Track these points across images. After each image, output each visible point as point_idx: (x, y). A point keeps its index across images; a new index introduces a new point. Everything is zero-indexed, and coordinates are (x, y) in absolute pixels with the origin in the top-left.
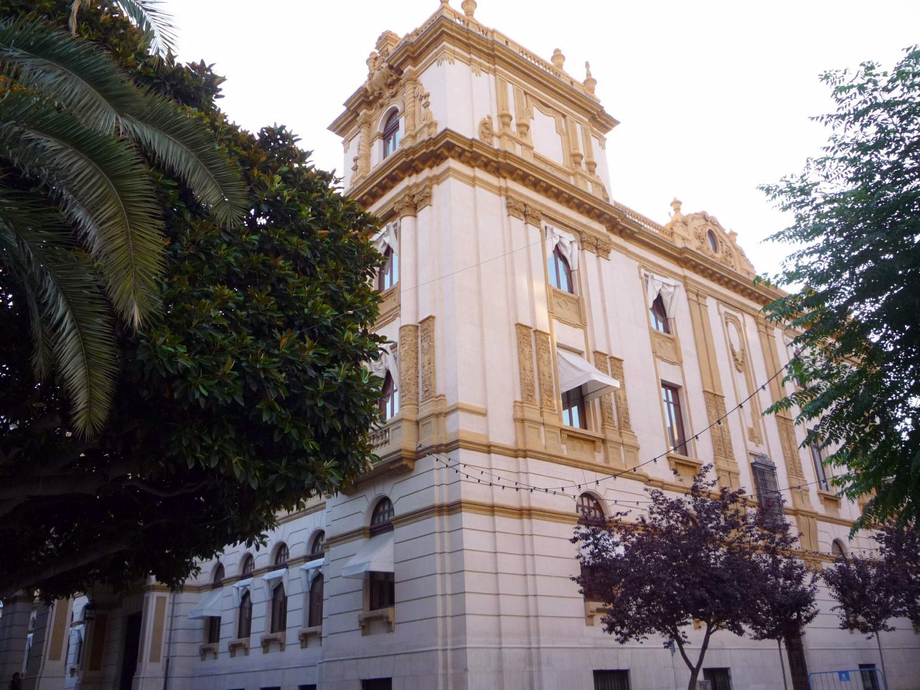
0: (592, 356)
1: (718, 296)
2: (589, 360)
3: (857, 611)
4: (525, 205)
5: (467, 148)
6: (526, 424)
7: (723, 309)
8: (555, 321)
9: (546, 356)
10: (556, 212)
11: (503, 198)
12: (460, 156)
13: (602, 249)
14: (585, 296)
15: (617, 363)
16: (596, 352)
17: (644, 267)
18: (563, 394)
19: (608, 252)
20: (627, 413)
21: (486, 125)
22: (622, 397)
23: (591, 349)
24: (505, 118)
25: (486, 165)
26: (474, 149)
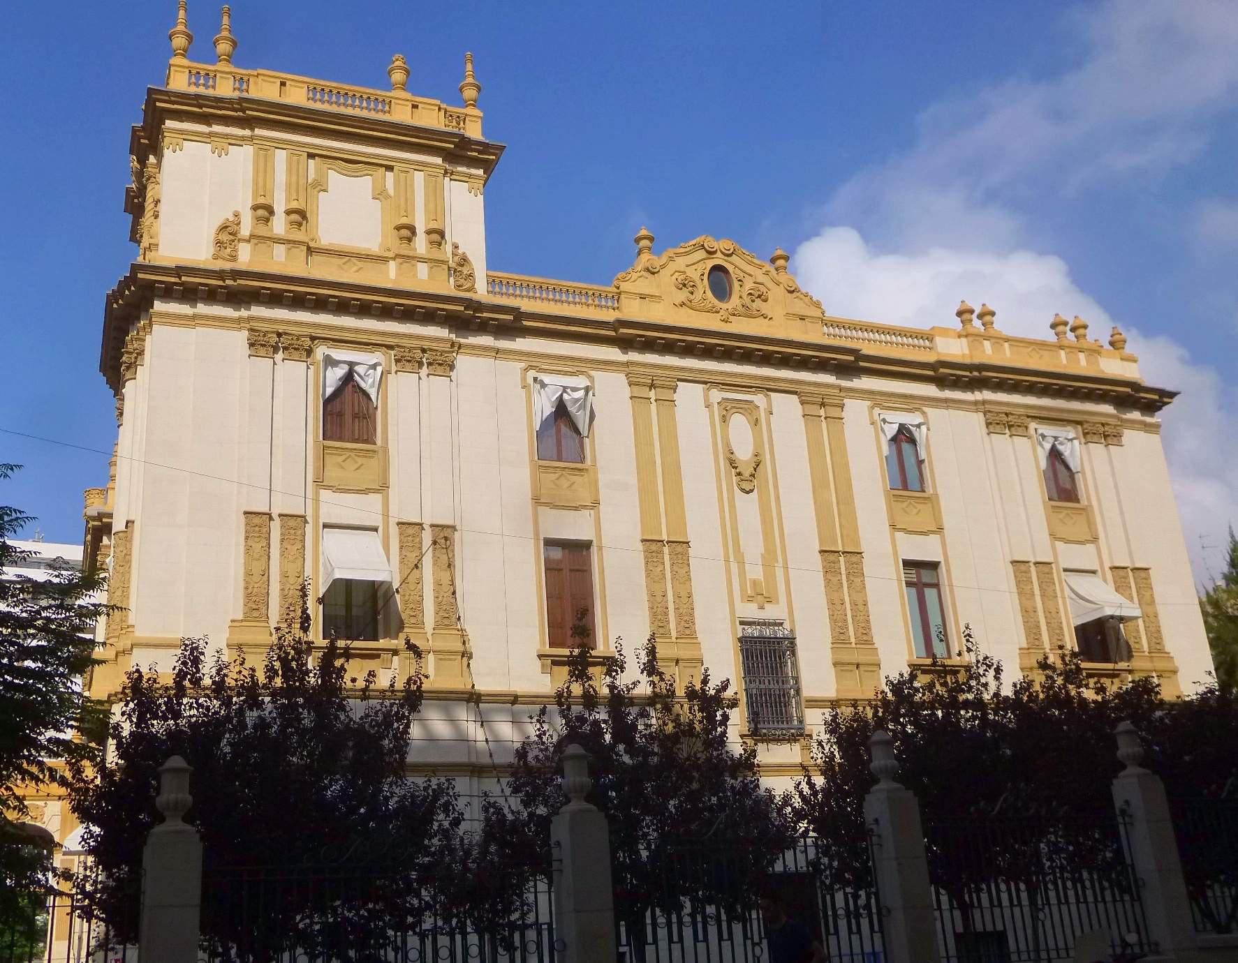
0: (1109, 573)
1: (706, 377)
2: (1105, 581)
3: (821, 826)
4: (1007, 414)
5: (173, 280)
6: (862, 668)
7: (716, 395)
8: (1059, 544)
9: (1148, 594)
10: (342, 329)
11: (981, 415)
12: (168, 293)
13: (1109, 435)
14: (1095, 503)
15: (1143, 574)
16: (1113, 568)
17: (878, 405)
18: (1077, 628)
19: (1118, 436)
20: (1159, 632)
21: (228, 233)
22: (860, 603)
23: (1107, 565)
24: (265, 211)
25: (212, 296)
26: (183, 279)
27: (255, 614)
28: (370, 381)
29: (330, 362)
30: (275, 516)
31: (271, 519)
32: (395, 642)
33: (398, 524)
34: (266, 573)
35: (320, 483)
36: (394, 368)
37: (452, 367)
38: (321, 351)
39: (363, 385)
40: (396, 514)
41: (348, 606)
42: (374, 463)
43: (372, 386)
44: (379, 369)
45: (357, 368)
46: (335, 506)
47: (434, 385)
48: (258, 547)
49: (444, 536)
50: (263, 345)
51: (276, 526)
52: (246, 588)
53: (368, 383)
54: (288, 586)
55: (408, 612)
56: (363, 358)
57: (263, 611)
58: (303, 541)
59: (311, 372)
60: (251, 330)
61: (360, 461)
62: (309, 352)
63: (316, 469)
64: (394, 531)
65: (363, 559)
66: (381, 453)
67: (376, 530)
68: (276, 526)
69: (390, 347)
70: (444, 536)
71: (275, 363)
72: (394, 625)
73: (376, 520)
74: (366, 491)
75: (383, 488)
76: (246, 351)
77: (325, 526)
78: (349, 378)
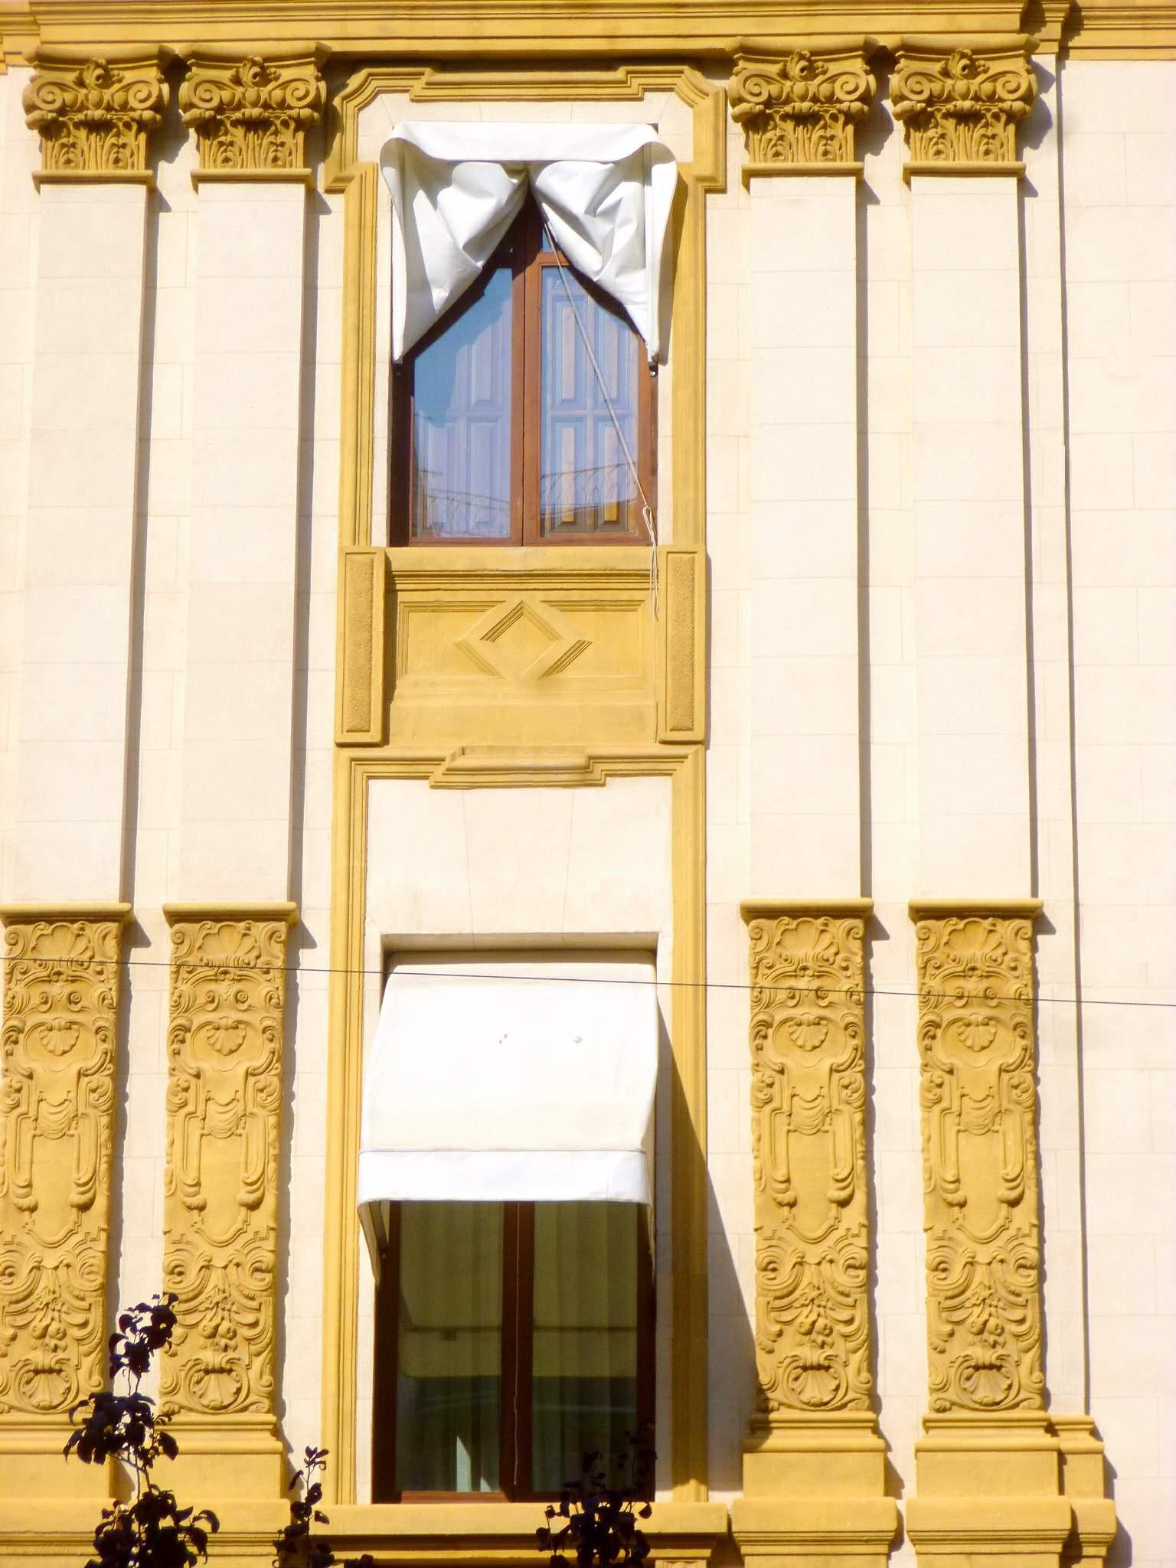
27: (986, 1388)
28: (624, 238)
29: (422, 172)
30: (892, 913)
31: (130, 933)
32: (724, 1499)
33: (753, 913)
34: (858, 1190)
35: (371, 748)
36: (739, 153)
37: (1030, 123)
38: (381, 119)
39: (587, 259)
40: (741, 876)
41: (518, 1328)
42: (641, 634)
43: (635, 261)
44: (664, 176)
45: (545, 181)
46: (432, 856)
47: (939, 222)
48: (812, 1069)
49: (990, 946)
50: (98, 127)
51: (897, 962)
52: (940, 1267)
53: (614, 242)
54: (965, 1247)
55: (787, 1347)
56: (572, 140)
57: (1024, 1374)
58: (863, 1028)
59: (333, 228)
60: (43, 60)
61: (571, 627)
62: (322, 130)
63: (353, 677)
64: (731, 949)
65: (512, 1105)
66: (666, 582)
67: (646, 952)
68: (897, 962)
69: (714, 63)
70: (990, 946)
71: (865, 196)
72: (724, 1413)
73: (640, 903)
74: (587, 773)
75: (681, 745)
76: (28, 152)
77: (394, 954)
78: (521, 234)
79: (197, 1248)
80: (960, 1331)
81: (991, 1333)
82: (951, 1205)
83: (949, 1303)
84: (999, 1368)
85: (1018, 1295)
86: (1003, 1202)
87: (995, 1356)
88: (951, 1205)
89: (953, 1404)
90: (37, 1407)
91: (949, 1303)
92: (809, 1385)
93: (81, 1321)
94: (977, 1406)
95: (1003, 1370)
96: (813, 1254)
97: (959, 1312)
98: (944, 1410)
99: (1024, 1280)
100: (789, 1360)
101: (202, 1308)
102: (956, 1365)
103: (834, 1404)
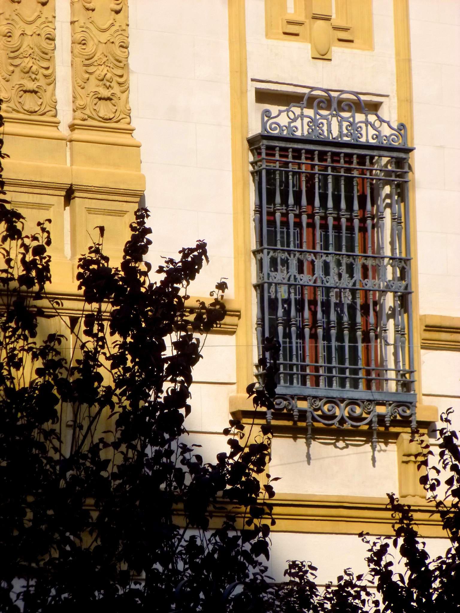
79: (17, 24)
80: (92, 78)
81: (33, 73)
82: (88, 9)
83: (12, 55)
84: (36, 92)
85: (120, 62)
86: (112, 11)
87: (35, 86)
88: (88, 9)
89: (89, 117)
90: (27, 111)
91: (12, 55)
92: (102, 107)
93: (120, 74)
94: (101, 119)
95: (38, 94)
96: (29, 30)
97: (92, 67)
98: (84, 120)
99: (122, 53)
100: (18, 86)
101: (95, 64)
102: (91, 95)
103: (115, 120)
